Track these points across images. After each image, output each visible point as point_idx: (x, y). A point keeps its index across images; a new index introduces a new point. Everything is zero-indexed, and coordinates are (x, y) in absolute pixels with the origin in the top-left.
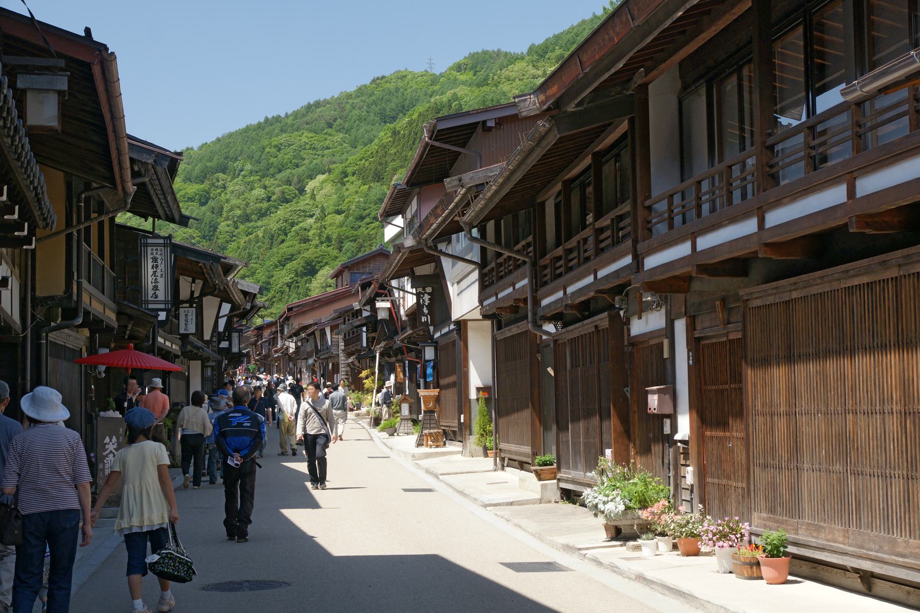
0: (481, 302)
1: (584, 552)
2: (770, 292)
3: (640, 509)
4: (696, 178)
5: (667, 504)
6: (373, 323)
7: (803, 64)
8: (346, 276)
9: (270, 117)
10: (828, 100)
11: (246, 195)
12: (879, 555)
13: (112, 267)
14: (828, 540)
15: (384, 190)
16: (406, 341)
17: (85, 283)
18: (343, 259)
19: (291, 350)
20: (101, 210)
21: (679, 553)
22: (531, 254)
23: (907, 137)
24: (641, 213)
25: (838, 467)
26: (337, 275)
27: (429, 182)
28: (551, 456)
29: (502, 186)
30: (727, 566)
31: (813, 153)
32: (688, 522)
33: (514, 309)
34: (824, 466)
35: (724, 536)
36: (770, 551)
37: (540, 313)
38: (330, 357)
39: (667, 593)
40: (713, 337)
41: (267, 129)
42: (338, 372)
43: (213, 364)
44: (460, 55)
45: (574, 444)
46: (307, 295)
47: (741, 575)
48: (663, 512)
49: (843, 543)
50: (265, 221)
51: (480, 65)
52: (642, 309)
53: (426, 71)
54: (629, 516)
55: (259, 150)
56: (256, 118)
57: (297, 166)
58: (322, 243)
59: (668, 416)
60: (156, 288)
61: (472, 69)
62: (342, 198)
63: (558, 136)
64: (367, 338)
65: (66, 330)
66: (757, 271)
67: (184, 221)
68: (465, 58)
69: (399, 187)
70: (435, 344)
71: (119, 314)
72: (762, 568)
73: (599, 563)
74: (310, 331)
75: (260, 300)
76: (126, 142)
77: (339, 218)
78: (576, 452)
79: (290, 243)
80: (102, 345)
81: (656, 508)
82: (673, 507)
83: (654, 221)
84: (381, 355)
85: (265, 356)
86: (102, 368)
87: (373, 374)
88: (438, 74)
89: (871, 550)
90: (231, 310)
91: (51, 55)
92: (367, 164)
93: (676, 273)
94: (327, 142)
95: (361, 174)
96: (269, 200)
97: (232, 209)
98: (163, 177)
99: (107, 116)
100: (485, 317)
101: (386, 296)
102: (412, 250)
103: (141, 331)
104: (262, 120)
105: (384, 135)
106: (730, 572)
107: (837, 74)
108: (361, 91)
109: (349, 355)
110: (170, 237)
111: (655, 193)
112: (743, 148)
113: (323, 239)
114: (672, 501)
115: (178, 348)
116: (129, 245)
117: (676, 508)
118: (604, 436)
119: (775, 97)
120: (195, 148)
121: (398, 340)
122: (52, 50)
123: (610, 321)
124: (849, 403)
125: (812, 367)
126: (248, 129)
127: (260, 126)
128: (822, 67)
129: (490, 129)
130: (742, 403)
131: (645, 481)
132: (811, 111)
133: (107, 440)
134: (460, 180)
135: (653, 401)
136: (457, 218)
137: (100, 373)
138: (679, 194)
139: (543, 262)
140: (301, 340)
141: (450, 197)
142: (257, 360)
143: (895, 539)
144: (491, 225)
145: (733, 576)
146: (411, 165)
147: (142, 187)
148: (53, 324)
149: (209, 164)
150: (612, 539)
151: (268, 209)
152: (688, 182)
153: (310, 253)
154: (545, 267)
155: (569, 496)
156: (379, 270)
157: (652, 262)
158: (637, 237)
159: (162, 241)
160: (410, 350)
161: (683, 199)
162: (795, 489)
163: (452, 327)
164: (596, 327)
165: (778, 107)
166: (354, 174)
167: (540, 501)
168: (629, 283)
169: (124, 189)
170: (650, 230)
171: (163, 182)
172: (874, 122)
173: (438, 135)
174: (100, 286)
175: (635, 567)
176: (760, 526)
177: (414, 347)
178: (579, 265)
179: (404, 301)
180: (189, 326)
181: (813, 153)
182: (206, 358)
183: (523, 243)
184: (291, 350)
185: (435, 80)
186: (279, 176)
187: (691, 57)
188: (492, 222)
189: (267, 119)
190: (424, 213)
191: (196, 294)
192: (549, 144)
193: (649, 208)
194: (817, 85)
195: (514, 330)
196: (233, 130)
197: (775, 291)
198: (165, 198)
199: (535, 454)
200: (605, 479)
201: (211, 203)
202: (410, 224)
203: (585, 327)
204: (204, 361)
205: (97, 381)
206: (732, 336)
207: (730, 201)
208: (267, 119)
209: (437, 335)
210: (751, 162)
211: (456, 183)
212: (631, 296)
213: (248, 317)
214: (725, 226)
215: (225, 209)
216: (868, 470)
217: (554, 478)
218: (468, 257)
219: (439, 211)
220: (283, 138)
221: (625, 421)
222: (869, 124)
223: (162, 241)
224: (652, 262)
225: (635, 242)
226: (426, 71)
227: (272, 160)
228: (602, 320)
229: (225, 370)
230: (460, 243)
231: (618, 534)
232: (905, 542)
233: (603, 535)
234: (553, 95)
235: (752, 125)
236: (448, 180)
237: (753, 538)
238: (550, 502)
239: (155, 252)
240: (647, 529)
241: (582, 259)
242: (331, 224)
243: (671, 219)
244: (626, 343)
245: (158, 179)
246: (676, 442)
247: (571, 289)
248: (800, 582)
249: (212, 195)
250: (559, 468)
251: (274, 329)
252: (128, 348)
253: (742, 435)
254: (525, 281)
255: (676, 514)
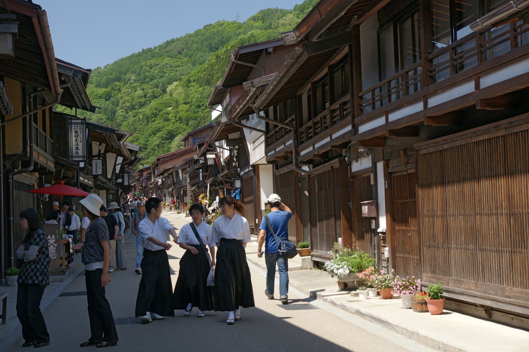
0: (266, 153)
1: (326, 298)
2: (431, 145)
3: (358, 272)
4: (388, 79)
5: (373, 269)
6: (205, 167)
7: (449, 11)
8: (191, 140)
9: (145, 49)
10: (463, 33)
11: (132, 94)
12: (496, 297)
13: (51, 137)
14: (466, 289)
15: (210, 90)
16: (224, 177)
17: (34, 146)
18: (189, 130)
19: (159, 183)
20: (44, 103)
21: (381, 297)
22: (294, 126)
23: (509, 52)
24: (356, 99)
25: (471, 246)
26: (185, 139)
27: (236, 85)
28: (307, 242)
29: (276, 86)
30: (408, 304)
31: (455, 63)
32: (386, 280)
33: (285, 158)
34: (463, 246)
35: (406, 287)
36: (433, 296)
37: (300, 159)
38: (182, 187)
39: (373, 321)
40: (399, 172)
41: (143, 56)
42: (186, 196)
43: (113, 192)
44: (255, 12)
45: (320, 235)
46: (168, 151)
47: (416, 310)
48: (371, 274)
49: (475, 291)
50: (143, 109)
51: (266, 17)
52: (358, 156)
53: (235, 21)
54: (352, 277)
55: (137, 67)
56: (137, 50)
57: (162, 77)
58: (177, 121)
59: (374, 218)
60: (77, 148)
61: (261, 19)
62: (187, 96)
63: (308, 56)
64: (203, 176)
65: (24, 174)
66: (423, 134)
67: (93, 109)
68: (258, 13)
69: (219, 88)
70: (241, 178)
71: (56, 164)
72: (428, 305)
73: (334, 304)
74: (170, 172)
75: (140, 155)
76: (56, 62)
77: (186, 107)
78: (322, 240)
79: (159, 121)
80: (47, 182)
81: (367, 272)
82: (377, 271)
83: (364, 105)
84: (211, 185)
85: (144, 187)
86: (47, 196)
87: (206, 196)
88: (242, 22)
89: (491, 294)
90: (123, 161)
91: (7, 12)
92: (202, 75)
93: (377, 135)
94: (179, 63)
95: (198, 80)
96: (145, 97)
97: (124, 103)
98: (79, 84)
99: (43, 49)
100: (269, 162)
101: (212, 151)
102: (226, 124)
103: (70, 174)
104: (141, 51)
105: (211, 58)
106: (410, 308)
107: (470, 17)
108: (197, 33)
109: (192, 185)
110: (85, 119)
111: (364, 89)
112: (415, 61)
113: (177, 119)
114: (376, 267)
115: (92, 183)
116: (61, 123)
117: (379, 271)
118: (337, 230)
119: (433, 31)
120: (103, 68)
121: (220, 177)
122: (8, 9)
123: (340, 164)
124: (478, 209)
125: (456, 188)
126: (132, 56)
127: (139, 54)
128: (460, 13)
129: (270, 53)
130: (416, 210)
131: (361, 256)
132: (454, 38)
133: (49, 237)
134: (252, 83)
135: (365, 209)
136: (251, 105)
137: (45, 198)
138: (379, 89)
139: (301, 130)
140: (165, 177)
141: (247, 93)
142: (140, 189)
143: (504, 287)
144: (271, 109)
145: (411, 310)
146: (225, 75)
147: (66, 90)
148: (16, 170)
149: (110, 77)
150: (342, 290)
151: (145, 102)
152: (383, 82)
153: (170, 127)
154: (302, 133)
155: (318, 265)
156: (207, 138)
157: (363, 129)
158: (354, 114)
159: (80, 121)
160: (227, 182)
161: (381, 92)
162: (447, 260)
163: (250, 168)
164: (332, 167)
165: (435, 37)
166: (194, 81)
167: (302, 268)
168: (350, 142)
169: (55, 91)
170: (362, 110)
171: (79, 87)
172: (491, 44)
173: (240, 57)
174: (44, 148)
175: (355, 306)
176: (427, 281)
177: (229, 181)
178: (321, 131)
179: (223, 154)
180: (98, 171)
181: (455, 63)
182: (109, 189)
183: (289, 119)
184: (159, 183)
185: (240, 26)
186: (151, 83)
187: (384, 8)
188: (272, 107)
189: (143, 50)
190: (234, 102)
191: (102, 152)
192: (302, 61)
193: (361, 98)
194: (458, 24)
195: (285, 170)
196: (124, 56)
197: (434, 145)
198: (81, 96)
199: (298, 241)
200: (338, 255)
201: (112, 99)
202: (225, 109)
203: (326, 167)
204: (108, 190)
205: (44, 203)
206: (410, 171)
207: (407, 93)
208: (143, 50)
209: (242, 173)
210: (420, 69)
211: (250, 85)
212: (352, 149)
213: (134, 164)
214: (405, 107)
215: (120, 102)
216: (488, 248)
217: (309, 255)
218: (258, 128)
219: (240, 102)
220: (153, 62)
221: (349, 221)
222: (487, 45)
223: (80, 121)
224: (363, 129)
225: (353, 117)
226: (235, 21)
227: (147, 74)
228: (335, 163)
229: (121, 195)
230: (254, 120)
231: (346, 287)
232: (510, 289)
233: (337, 288)
234: (304, 32)
235: (420, 48)
236: (245, 83)
237: (423, 288)
238: (307, 269)
239: (76, 128)
240: (362, 284)
241: (323, 128)
242: (182, 111)
243: (374, 103)
244: (349, 176)
245: (76, 85)
246: (379, 233)
247: (317, 146)
248: (450, 313)
249: (112, 94)
250: (312, 249)
251: (149, 171)
252: (60, 183)
253: (416, 228)
254: (291, 141)
255: (379, 275)
